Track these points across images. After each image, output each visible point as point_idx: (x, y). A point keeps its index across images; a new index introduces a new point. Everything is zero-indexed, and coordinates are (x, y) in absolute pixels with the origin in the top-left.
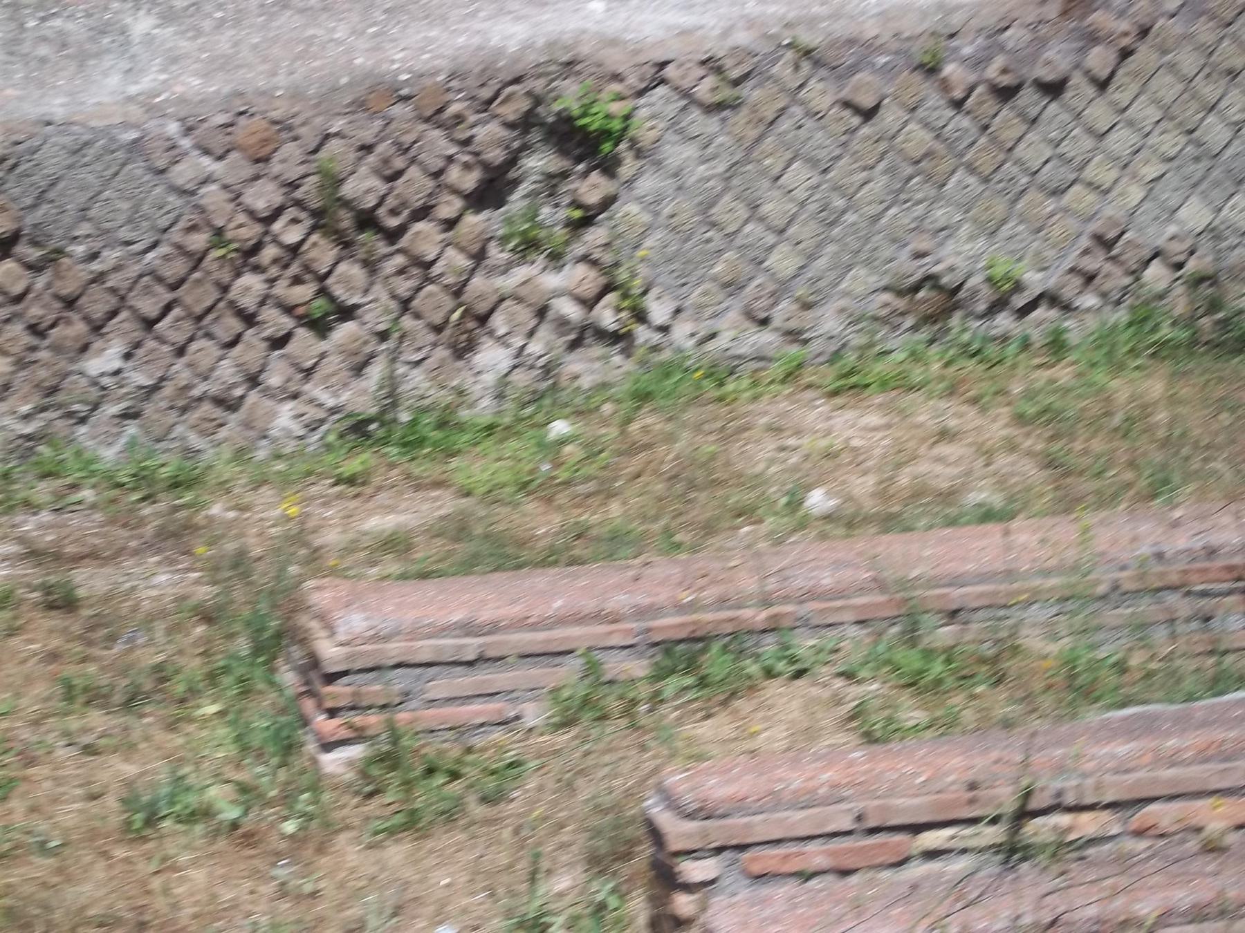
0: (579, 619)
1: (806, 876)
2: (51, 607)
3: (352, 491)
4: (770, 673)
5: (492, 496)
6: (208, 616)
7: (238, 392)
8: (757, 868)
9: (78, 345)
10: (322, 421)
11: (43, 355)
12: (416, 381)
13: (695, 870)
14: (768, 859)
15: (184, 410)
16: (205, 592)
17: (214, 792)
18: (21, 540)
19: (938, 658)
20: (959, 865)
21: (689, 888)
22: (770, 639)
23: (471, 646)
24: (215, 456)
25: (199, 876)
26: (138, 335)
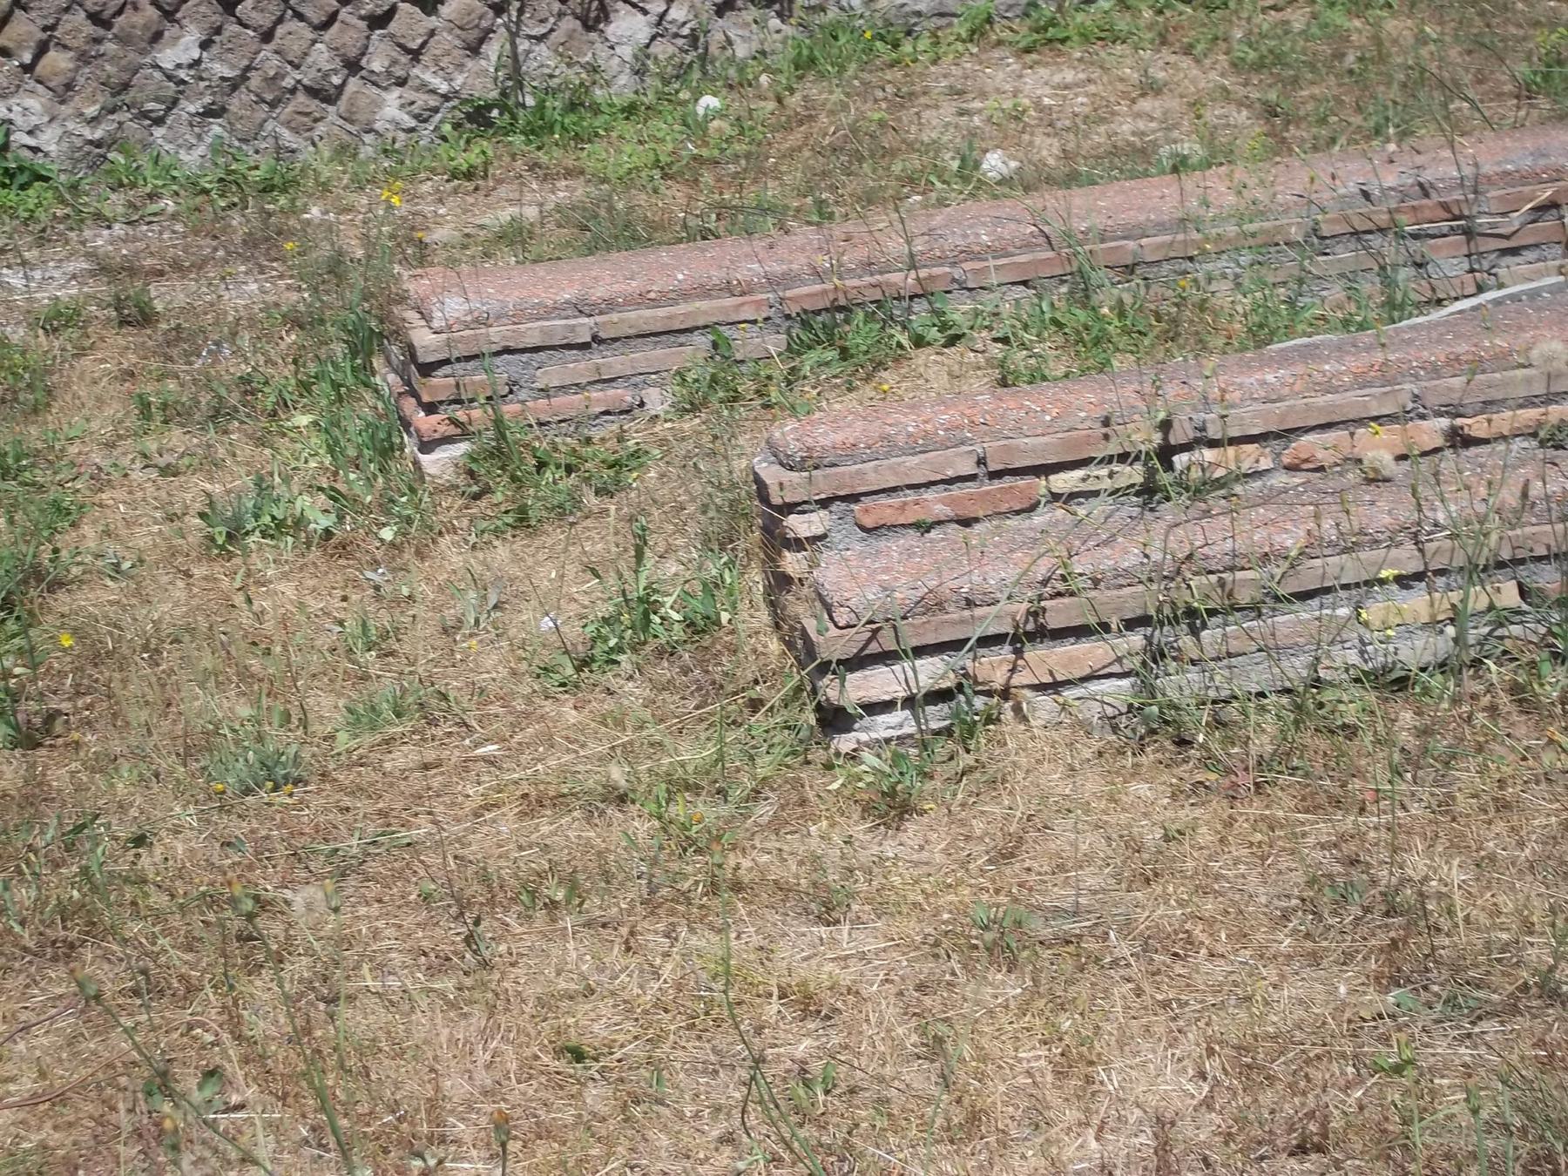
0: (705, 292)
1: (923, 527)
2: (124, 322)
3: (470, 186)
4: (919, 342)
5: (628, 180)
6: (295, 321)
7: (336, 80)
8: (869, 522)
9: (149, 35)
10: (436, 110)
11: (110, 47)
12: (541, 59)
13: (799, 525)
14: (882, 510)
15: (273, 105)
16: (296, 299)
17: (304, 502)
18: (91, 256)
19: (1102, 306)
20: (1099, 507)
21: (798, 544)
22: (920, 306)
23: (583, 328)
24: (315, 157)
25: (288, 589)
26: (217, 19)
